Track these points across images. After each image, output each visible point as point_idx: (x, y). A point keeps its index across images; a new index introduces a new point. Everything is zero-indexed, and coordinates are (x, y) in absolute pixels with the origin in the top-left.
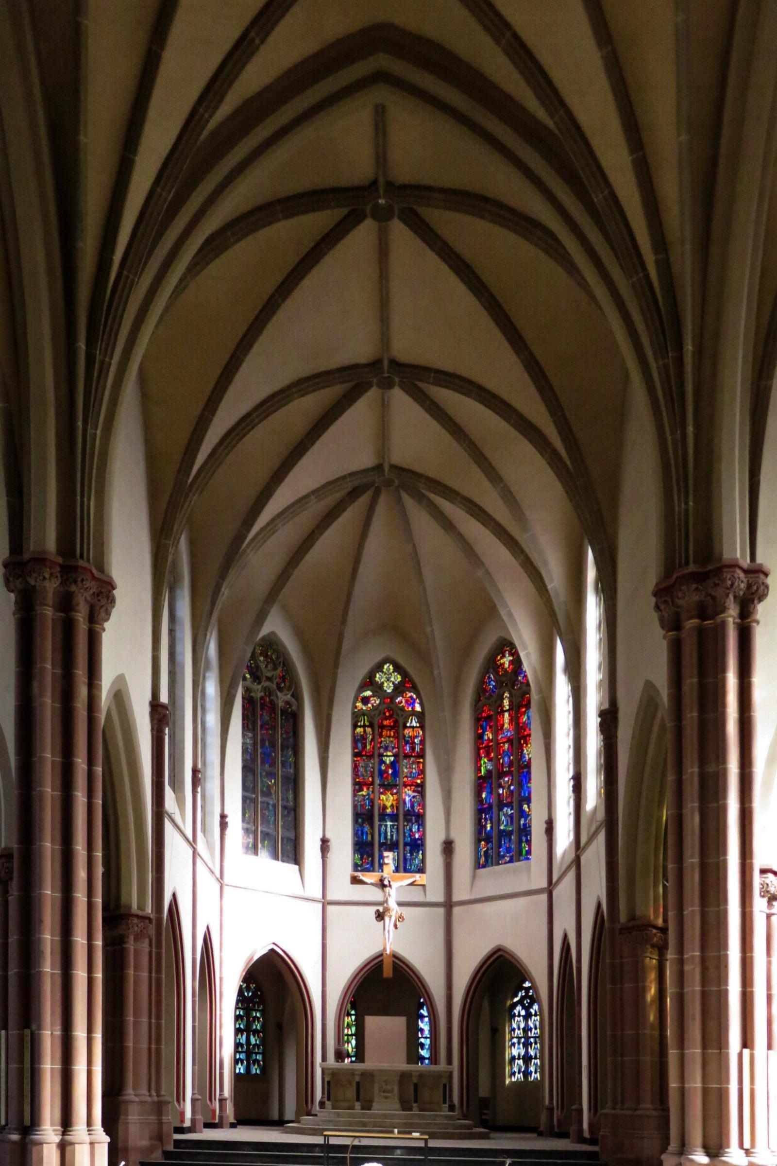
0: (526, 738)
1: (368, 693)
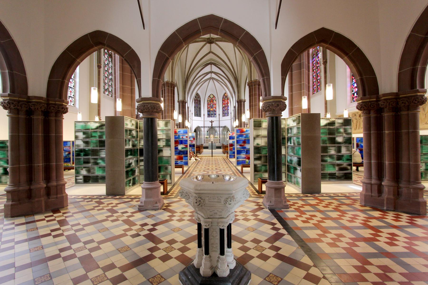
0: (228, 103)
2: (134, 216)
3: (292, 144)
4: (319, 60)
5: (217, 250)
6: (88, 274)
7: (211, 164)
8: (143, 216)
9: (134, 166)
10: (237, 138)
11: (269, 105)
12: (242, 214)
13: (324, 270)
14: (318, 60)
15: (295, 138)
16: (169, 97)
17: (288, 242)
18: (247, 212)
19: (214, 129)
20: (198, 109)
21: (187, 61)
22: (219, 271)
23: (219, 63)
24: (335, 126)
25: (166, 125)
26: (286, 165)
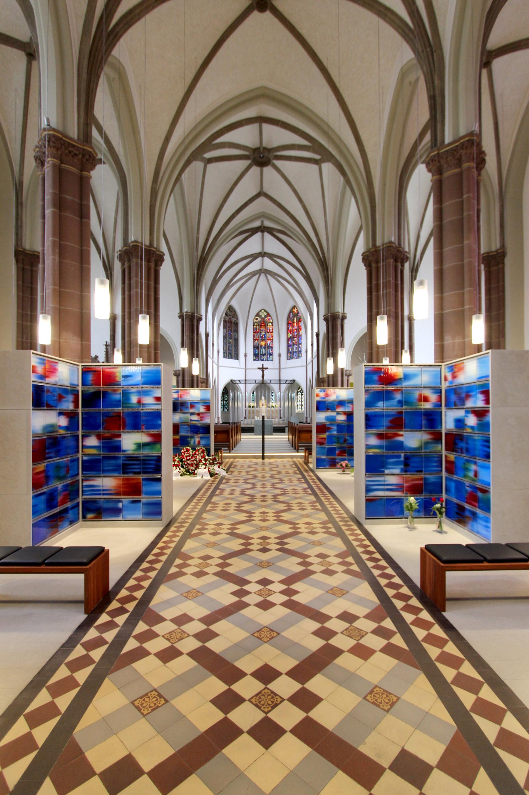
10: (368, 404)
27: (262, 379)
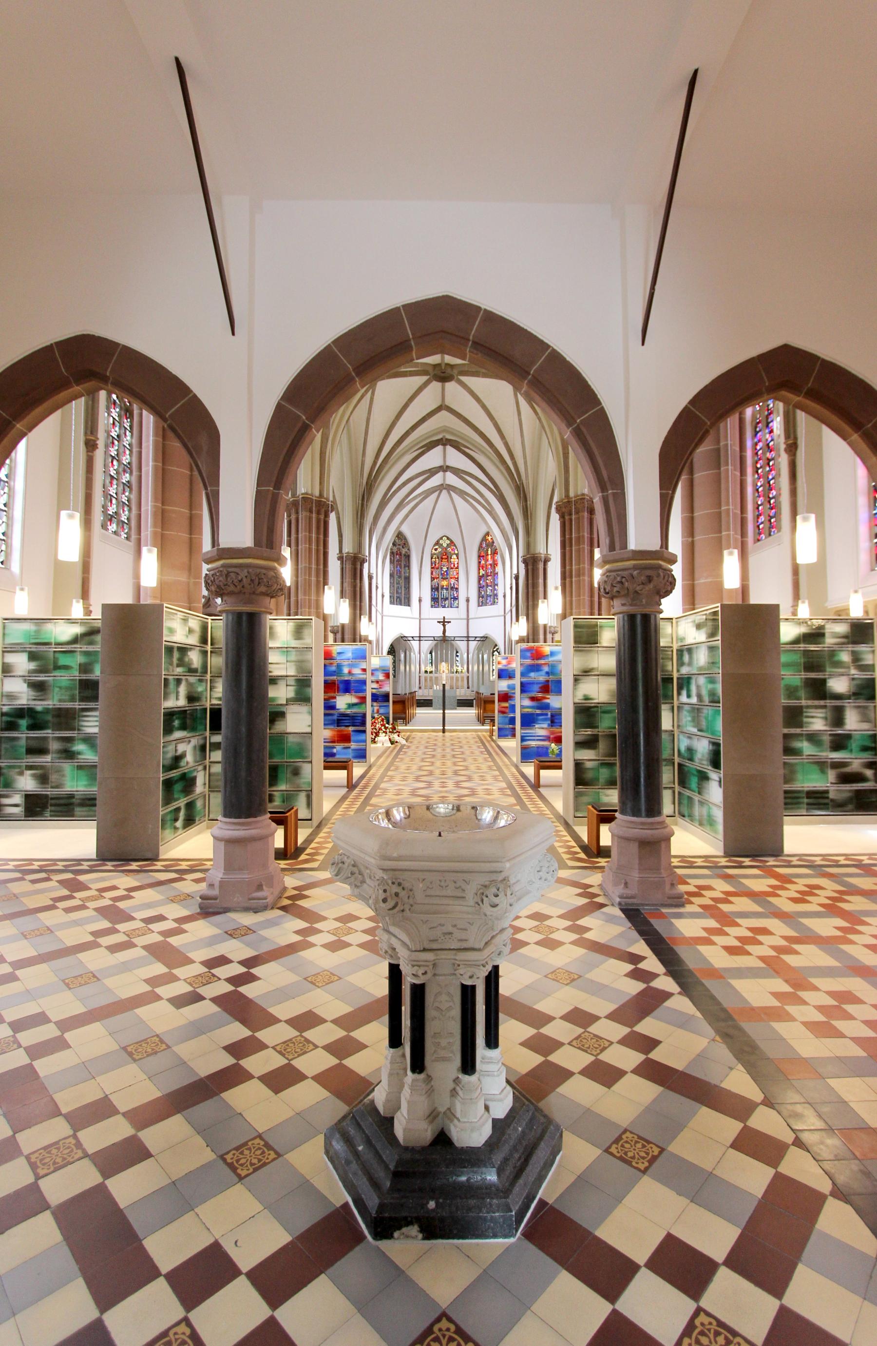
1: (437, 547)
2: (185, 931)
3: (694, 700)
4: (772, 440)
5: (451, 1055)
6: (20, 1137)
7: (439, 756)
8: (216, 931)
9: (191, 764)
10: (523, 674)
11: (623, 577)
12: (537, 923)
13: (797, 1116)
14: (770, 439)
15: (702, 680)
16: (310, 544)
17: (682, 1022)
18: (550, 917)
19: (452, 645)
20: (402, 582)
21: (370, 431)
22: (455, 1126)
23: (468, 441)
24: (824, 643)
25: (298, 632)
26: (674, 763)
27: (442, 635)
